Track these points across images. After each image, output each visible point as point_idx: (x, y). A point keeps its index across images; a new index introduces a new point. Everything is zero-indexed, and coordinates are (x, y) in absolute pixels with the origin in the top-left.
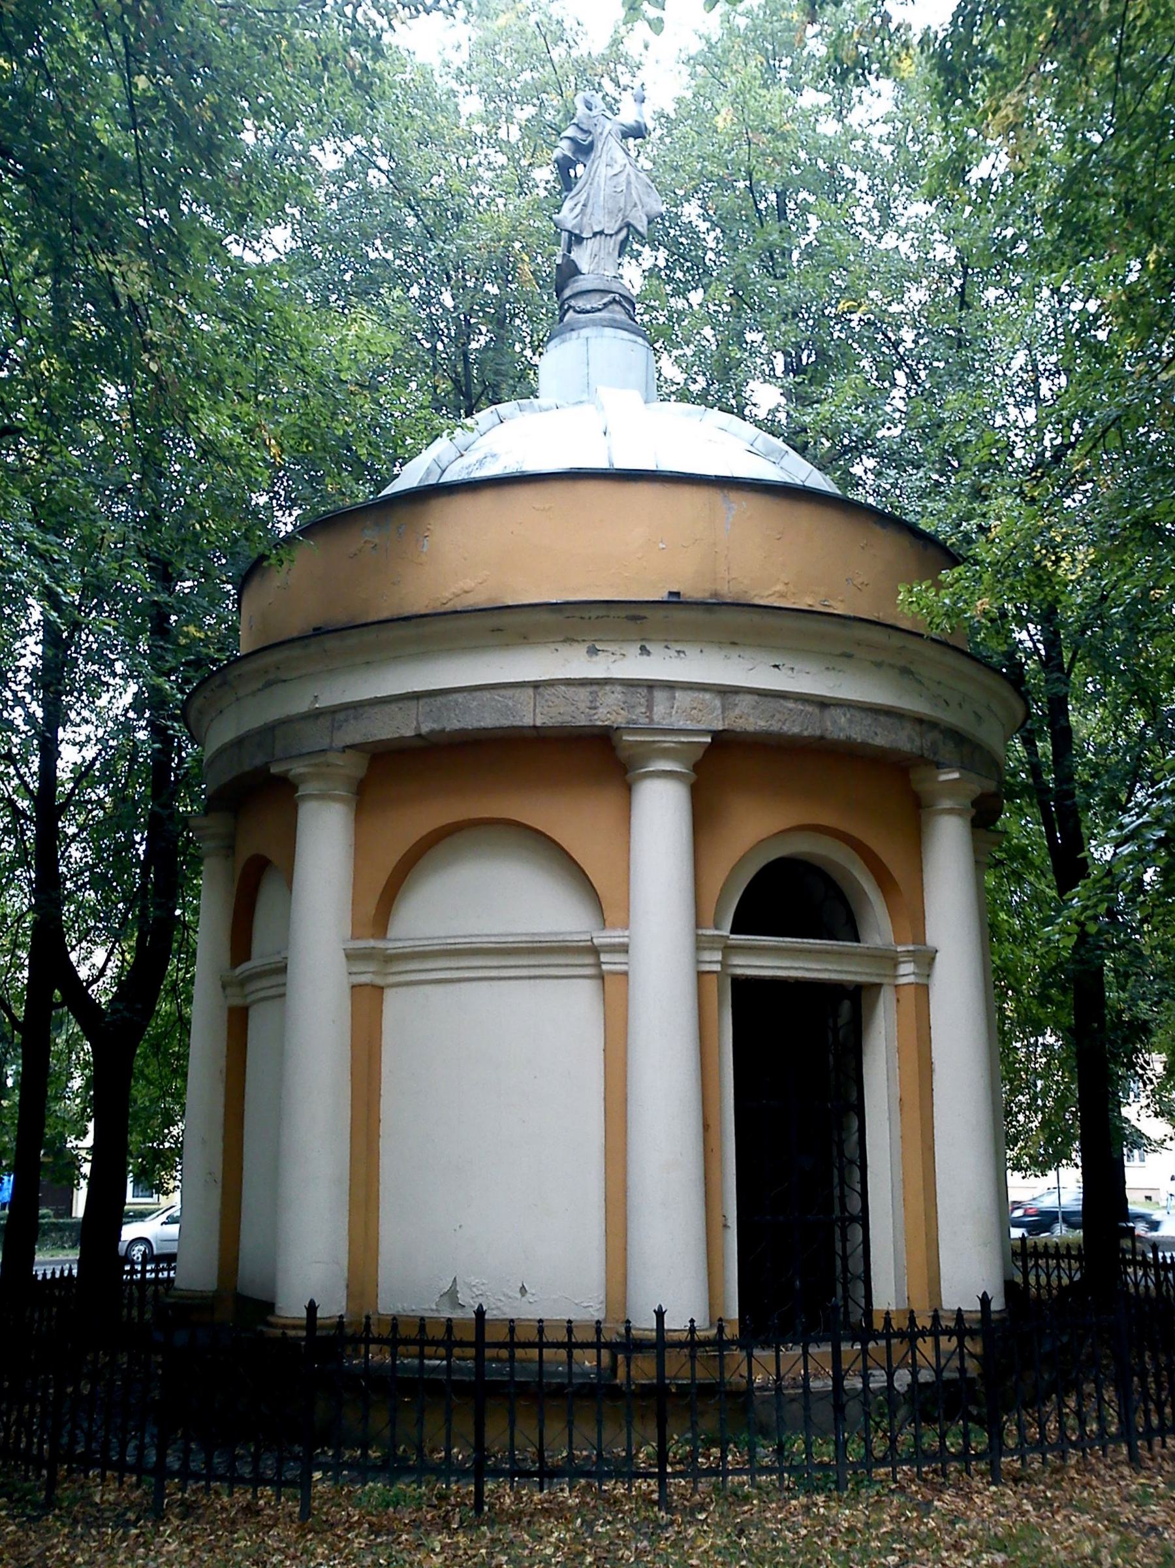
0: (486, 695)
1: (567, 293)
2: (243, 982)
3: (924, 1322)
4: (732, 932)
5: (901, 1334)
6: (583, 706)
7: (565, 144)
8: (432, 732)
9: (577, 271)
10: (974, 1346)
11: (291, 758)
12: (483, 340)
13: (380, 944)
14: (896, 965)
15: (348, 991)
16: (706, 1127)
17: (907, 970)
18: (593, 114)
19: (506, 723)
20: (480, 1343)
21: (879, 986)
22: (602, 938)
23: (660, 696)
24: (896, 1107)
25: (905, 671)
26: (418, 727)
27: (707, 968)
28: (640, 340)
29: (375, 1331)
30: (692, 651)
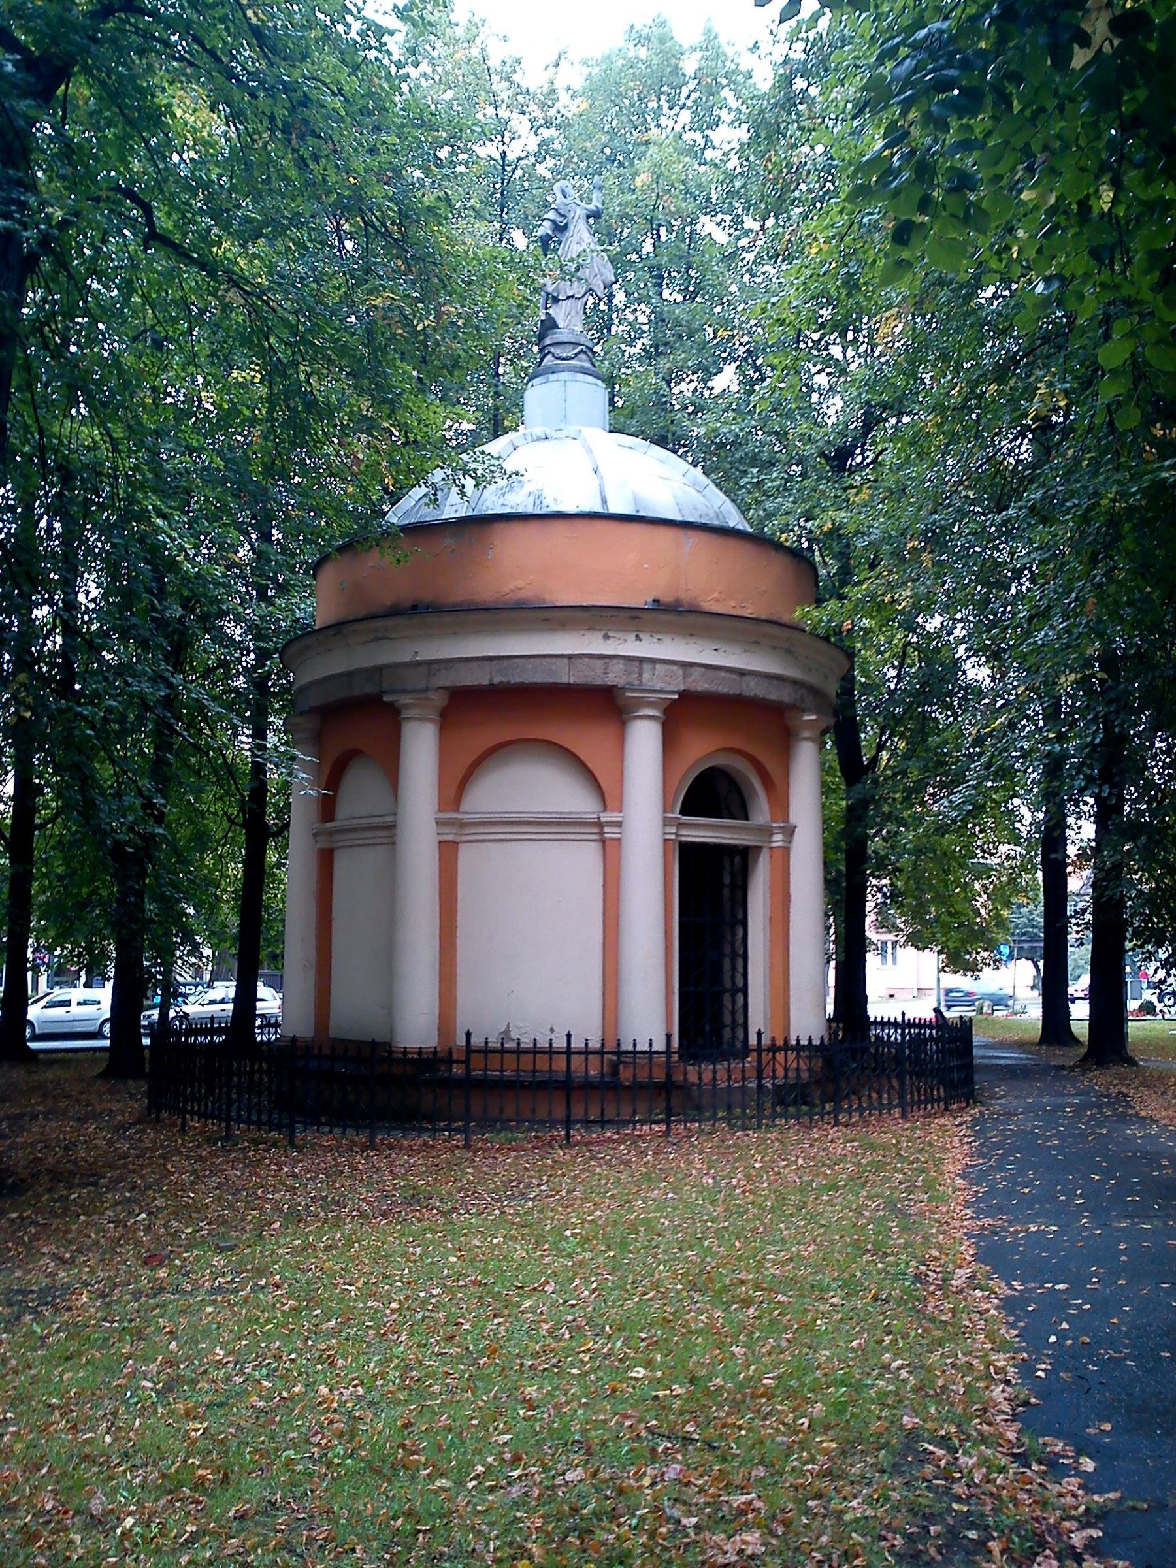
0: (538, 661)
1: (548, 341)
2: (330, 833)
4: (683, 812)
6: (600, 671)
7: (547, 224)
8: (501, 682)
9: (555, 326)
11: (404, 691)
13: (456, 816)
14: (771, 835)
15: (437, 845)
16: (666, 933)
17: (778, 838)
18: (567, 201)
19: (551, 680)
21: (761, 848)
22: (605, 818)
23: (646, 666)
24: (768, 921)
25: (789, 651)
26: (491, 679)
27: (668, 837)
28: (599, 382)
29: (455, 1057)
30: (667, 640)
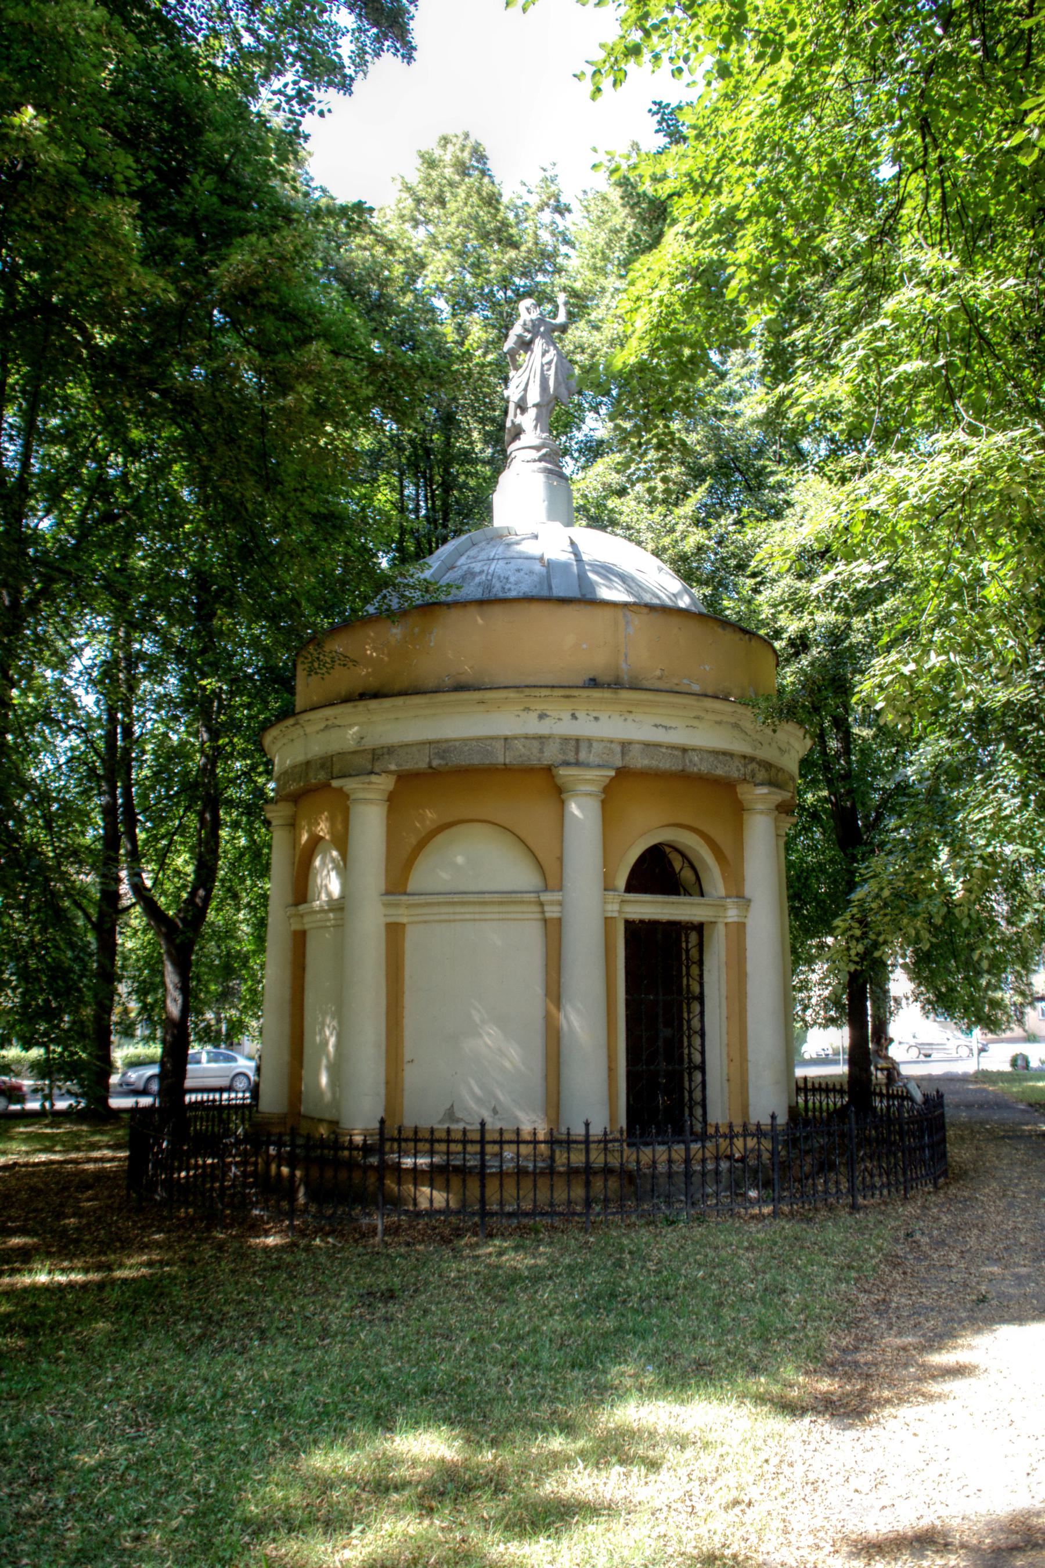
3: (738, 1129)
5: (725, 1136)
10: (767, 1144)
12: (959, 886)
20: (482, 1142)
